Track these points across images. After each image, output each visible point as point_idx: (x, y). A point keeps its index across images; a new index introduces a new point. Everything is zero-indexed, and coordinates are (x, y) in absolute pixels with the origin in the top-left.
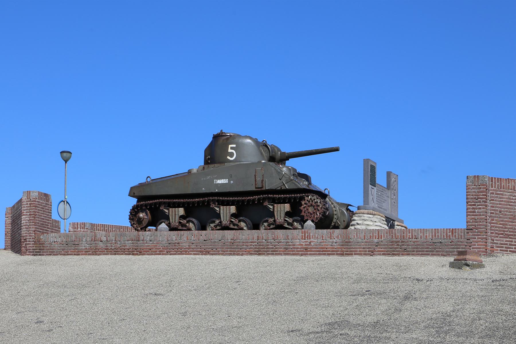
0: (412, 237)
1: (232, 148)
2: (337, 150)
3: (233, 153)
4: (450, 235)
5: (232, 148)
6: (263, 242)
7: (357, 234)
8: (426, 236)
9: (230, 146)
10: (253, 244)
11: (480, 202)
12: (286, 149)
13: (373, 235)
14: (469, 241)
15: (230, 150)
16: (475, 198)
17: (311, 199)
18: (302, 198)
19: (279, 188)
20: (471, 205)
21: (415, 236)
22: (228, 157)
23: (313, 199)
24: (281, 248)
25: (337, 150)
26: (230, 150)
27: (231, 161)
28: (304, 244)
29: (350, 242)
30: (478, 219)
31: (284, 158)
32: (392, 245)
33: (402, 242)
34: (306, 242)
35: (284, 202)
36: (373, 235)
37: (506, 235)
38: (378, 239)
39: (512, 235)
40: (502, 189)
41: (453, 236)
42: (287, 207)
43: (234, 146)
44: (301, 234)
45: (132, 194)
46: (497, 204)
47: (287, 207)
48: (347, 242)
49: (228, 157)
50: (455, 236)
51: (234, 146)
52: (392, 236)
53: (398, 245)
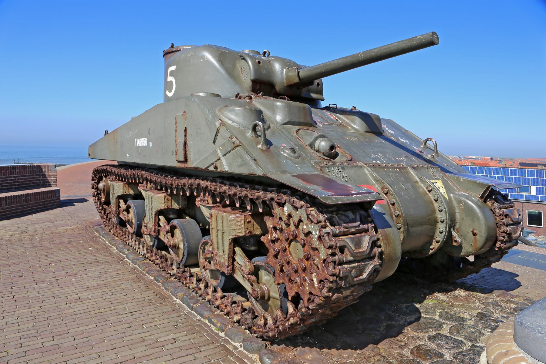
1: (172, 74)
5: (172, 74)
17: (290, 216)
23: (296, 219)
26: (170, 79)
31: (303, 91)
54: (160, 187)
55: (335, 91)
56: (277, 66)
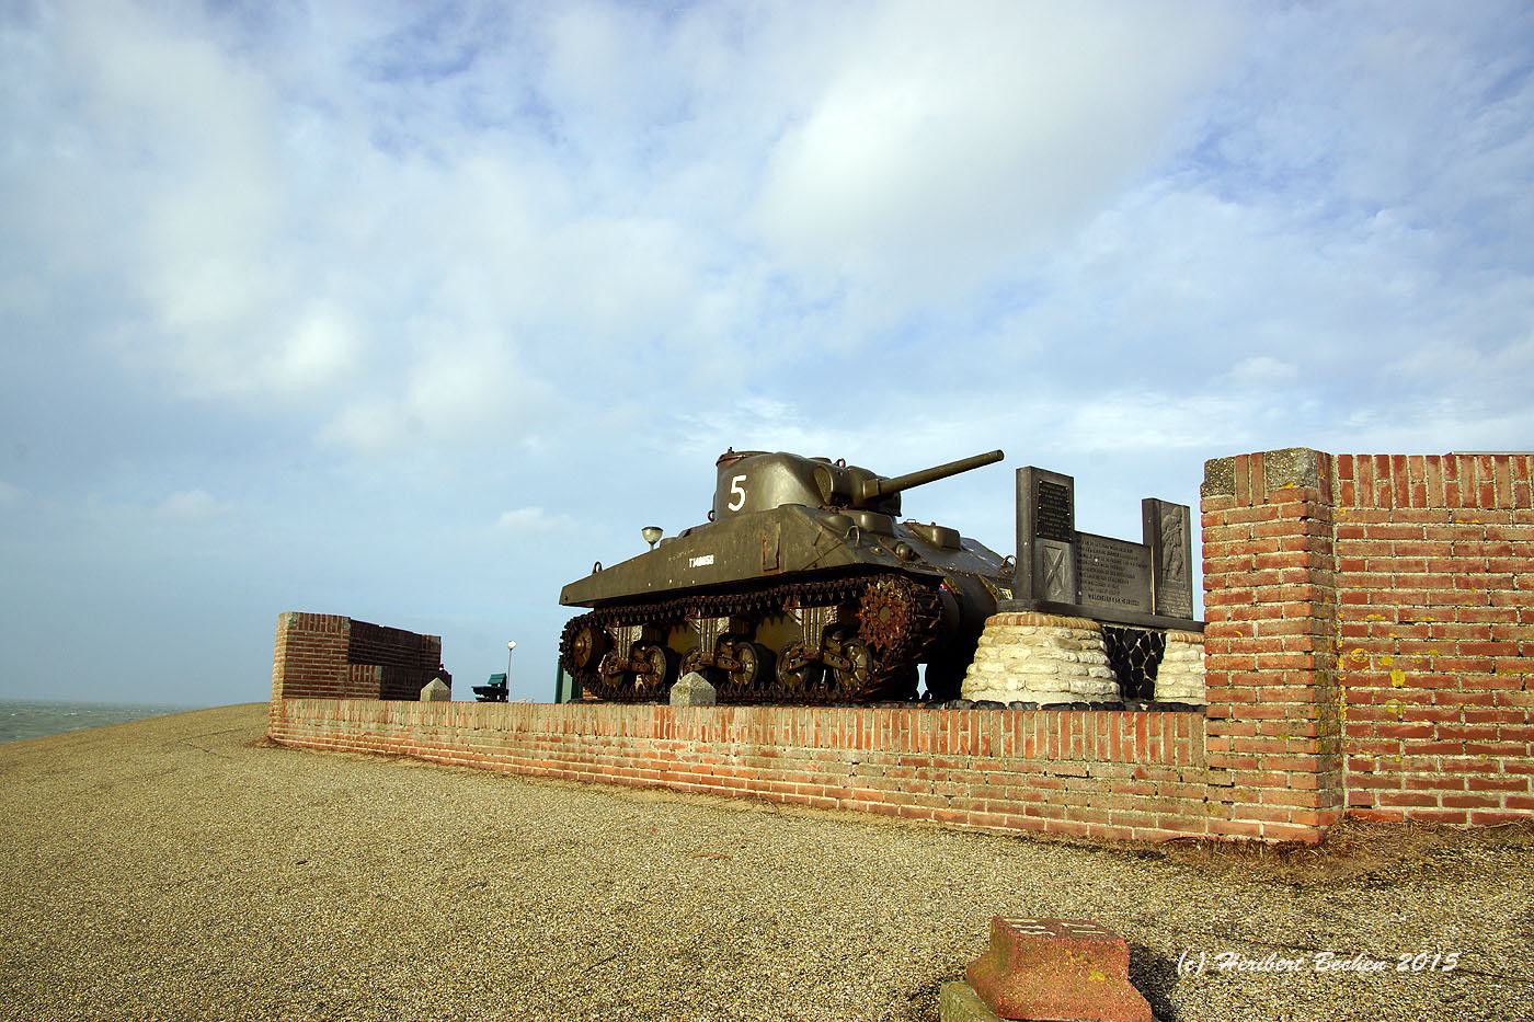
0: (975, 747)
1: (739, 484)
2: (997, 456)
3: (739, 495)
4: (1128, 745)
5: (739, 484)
6: (573, 741)
7: (794, 727)
8: (1029, 743)
9: (736, 479)
10: (557, 745)
11: (1271, 579)
12: (887, 465)
13: (842, 732)
14: (1219, 778)
15: (734, 490)
16: (1246, 565)
17: (881, 589)
18: (861, 591)
19: (811, 568)
20: (1225, 600)
21: (987, 741)
22: (731, 506)
24: (608, 762)
25: (997, 456)
26: (734, 490)
27: (736, 513)
28: (658, 752)
29: (773, 755)
30: (1263, 665)
31: (885, 498)
32: (904, 774)
33: (941, 764)
34: (665, 746)
35: (826, 603)
36: (842, 732)
37: (1445, 733)
38: (858, 747)
39: (1490, 735)
40: (1412, 509)
41: (1142, 752)
42: (830, 615)
43: (742, 478)
44: (652, 720)
45: (569, 597)
46: (1386, 582)
47: (830, 615)
48: (765, 754)
49: (731, 506)
50: (1154, 750)
51: (742, 478)
52: (905, 736)
53: (923, 776)
54: (713, 612)
55: (917, 508)
56: (856, 478)
